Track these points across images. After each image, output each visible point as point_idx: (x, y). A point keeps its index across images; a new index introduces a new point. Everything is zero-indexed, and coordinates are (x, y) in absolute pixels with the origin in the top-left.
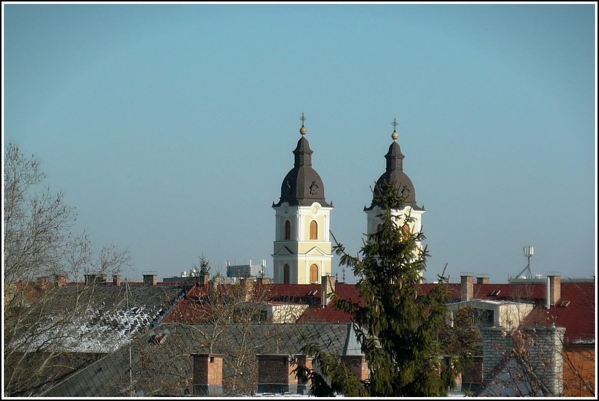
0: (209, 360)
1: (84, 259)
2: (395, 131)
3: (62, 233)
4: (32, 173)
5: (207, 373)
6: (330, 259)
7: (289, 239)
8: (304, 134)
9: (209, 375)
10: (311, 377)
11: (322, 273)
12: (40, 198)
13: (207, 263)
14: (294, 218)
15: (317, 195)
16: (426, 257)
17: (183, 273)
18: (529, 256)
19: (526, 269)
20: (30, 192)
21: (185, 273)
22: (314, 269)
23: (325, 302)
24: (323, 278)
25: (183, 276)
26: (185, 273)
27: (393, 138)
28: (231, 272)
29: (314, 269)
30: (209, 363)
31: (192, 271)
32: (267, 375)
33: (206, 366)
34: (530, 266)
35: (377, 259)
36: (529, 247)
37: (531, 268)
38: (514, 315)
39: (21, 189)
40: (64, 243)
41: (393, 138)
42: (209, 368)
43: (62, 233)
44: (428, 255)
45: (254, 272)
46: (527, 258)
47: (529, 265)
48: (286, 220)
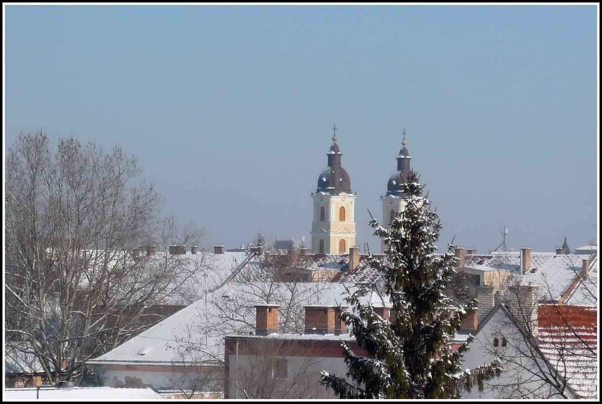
0: (268, 310)
1: (172, 234)
2: (404, 139)
3: (153, 213)
4: (132, 168)
5: (266, 320)
6: (354, 236)
7: (324, 220)
8: (335, 140)
9: (268, 322)
10: (352, 321)
11: (350, 245)
12: (138, 187)
13: (263, 238)
14: (328, 204)
15: (345, 187)
16: (439, 229)
17: (241, 246)
18: (505, 234)
19: (502, 244)
20: (130, 183)
21: (243, 246)
22: (343, 243)
23: (352, 268)
24: (351, 250)
25: (242, 248)
26: (243, 246)
27: (403, 144)
28: (279, 245)
29: (343, 243)
30: (268, 312)
31: (248, 245)
32: (312, 322)
33: (266, 315)
34: (505, 242)
35: (402, 232)
36: (505, 228)
37: (506, 245)
38: (496, 278)
39: (123, 181)
40: (156, 221)
41: (403, 144)
42: (268, 316)
43: (153, 213)
44: (441, 228)
45: (297, 245)
46: (503, 236)
47: (504, 241)
48: (321, 206)
